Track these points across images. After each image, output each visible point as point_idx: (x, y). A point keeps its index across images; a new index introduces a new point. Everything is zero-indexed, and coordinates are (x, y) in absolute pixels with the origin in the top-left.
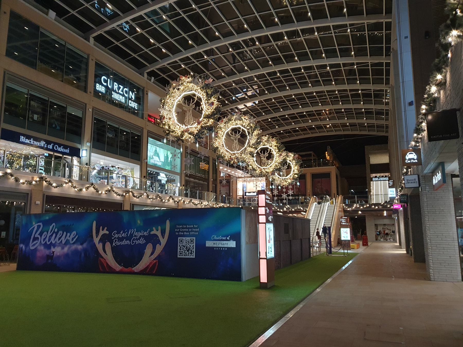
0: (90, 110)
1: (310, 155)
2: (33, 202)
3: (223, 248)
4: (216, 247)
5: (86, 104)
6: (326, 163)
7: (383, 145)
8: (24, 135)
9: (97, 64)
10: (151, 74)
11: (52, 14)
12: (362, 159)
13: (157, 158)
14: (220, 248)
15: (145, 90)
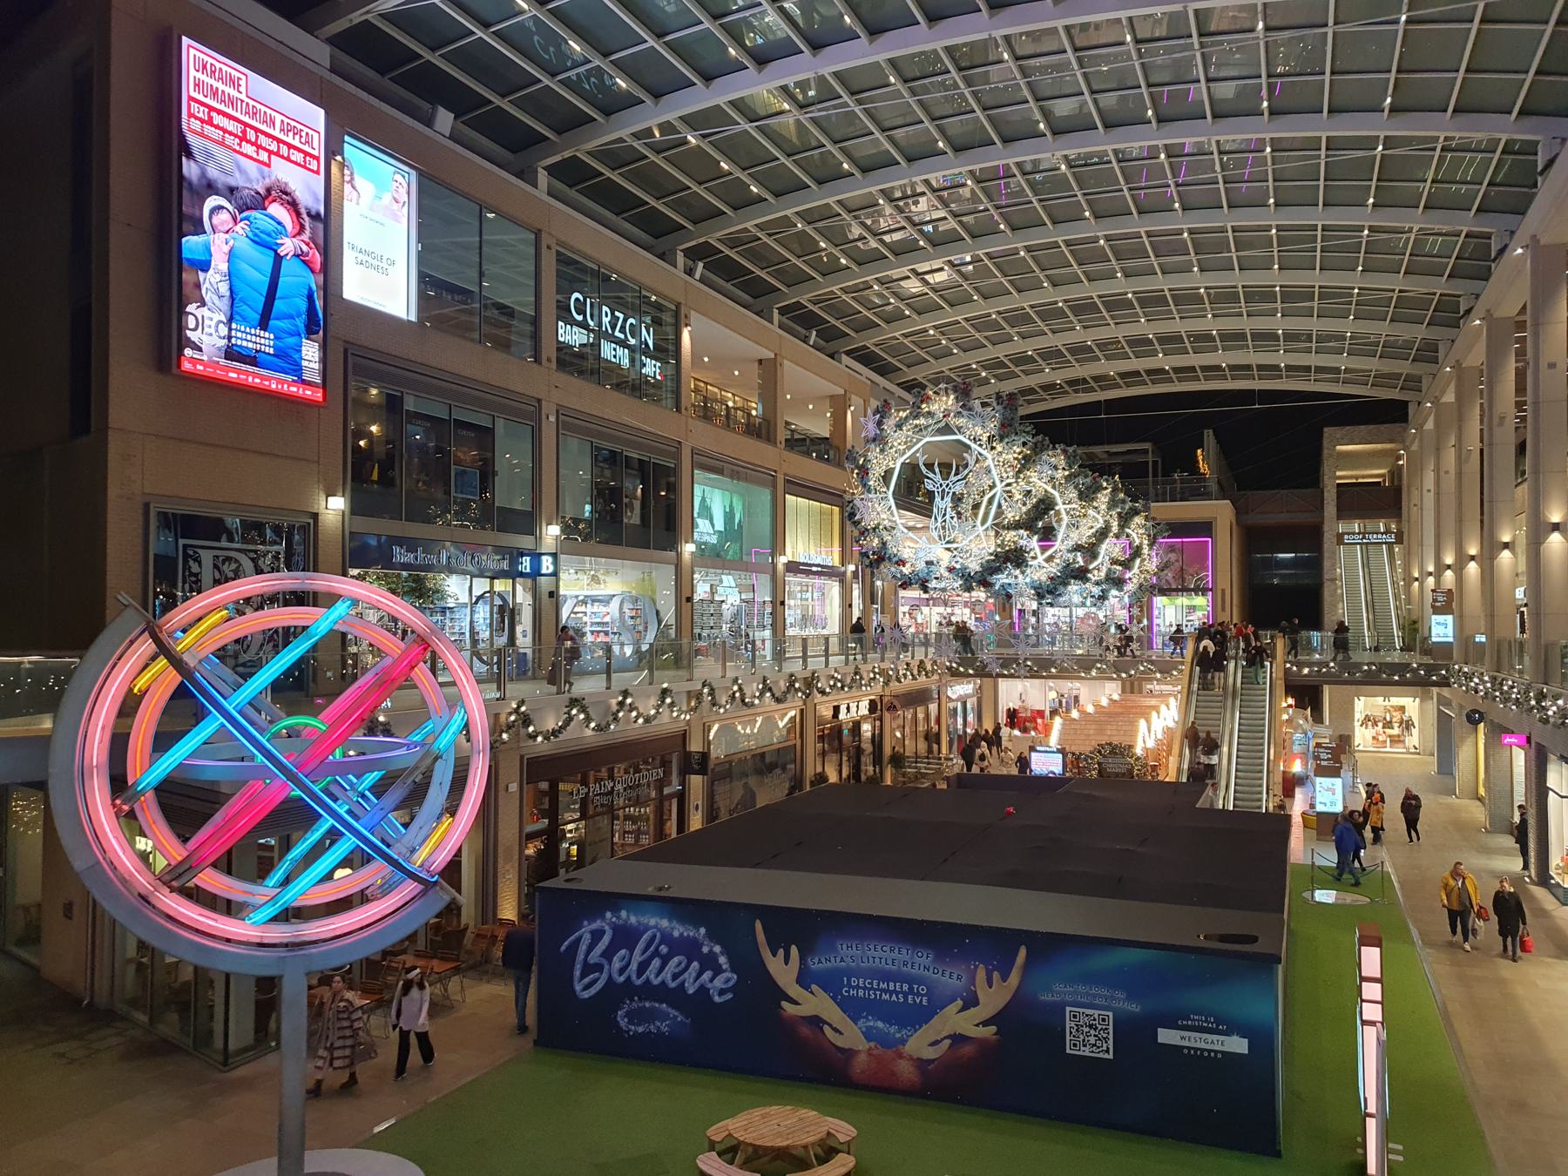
0: (552, 419)
1: (1145, 452)
2: (502, 786)
3: (1210, 1051)
4: (1189, 1048)
5: (539, 401)
6: (1196, 491)
7: (1383, 427)
8: (400, 541)
9: (562, 259)
10: (694, 254)
11: (445, 119)
12: (1305, 469)
13: (707, 522)
14: (1203, 1050)
15: (683, 311)
